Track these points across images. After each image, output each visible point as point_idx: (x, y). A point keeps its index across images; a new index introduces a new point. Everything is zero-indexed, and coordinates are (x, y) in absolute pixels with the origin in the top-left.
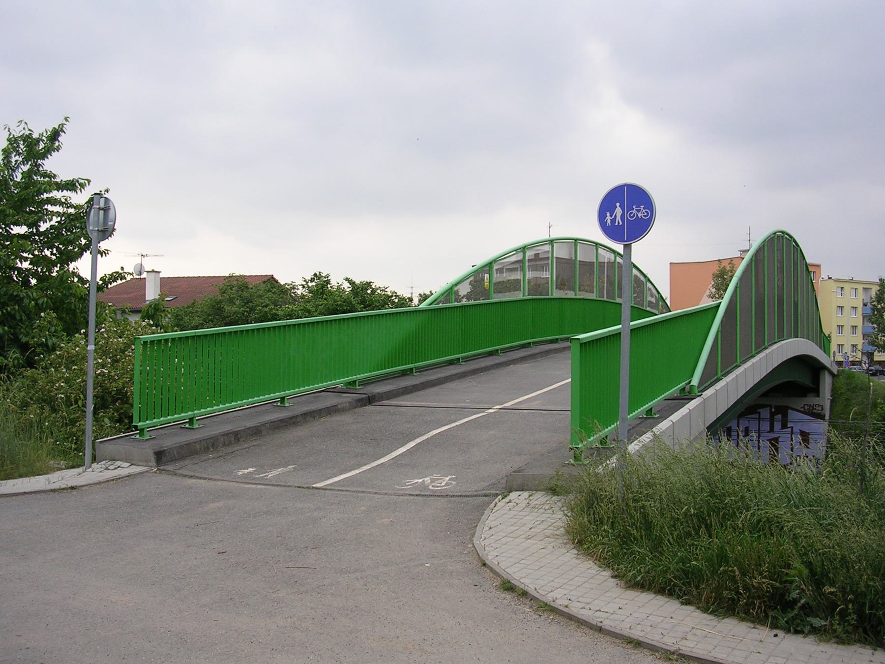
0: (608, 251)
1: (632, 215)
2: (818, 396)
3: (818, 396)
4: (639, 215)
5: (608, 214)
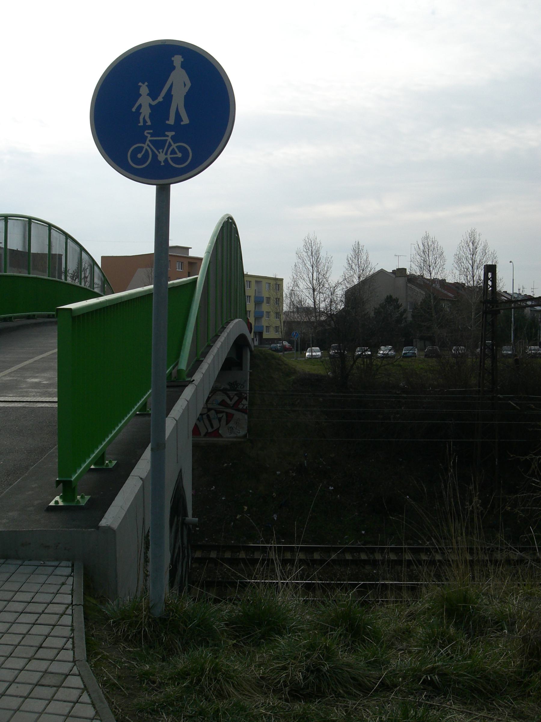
0: (61, 233)
1: (140, 156)
2: (242, 370)
3: (242, 370)
4: (161, 157)
5: (144, 89)
